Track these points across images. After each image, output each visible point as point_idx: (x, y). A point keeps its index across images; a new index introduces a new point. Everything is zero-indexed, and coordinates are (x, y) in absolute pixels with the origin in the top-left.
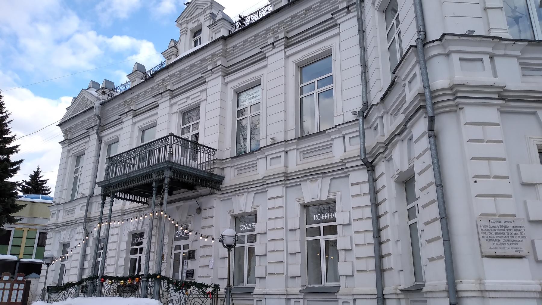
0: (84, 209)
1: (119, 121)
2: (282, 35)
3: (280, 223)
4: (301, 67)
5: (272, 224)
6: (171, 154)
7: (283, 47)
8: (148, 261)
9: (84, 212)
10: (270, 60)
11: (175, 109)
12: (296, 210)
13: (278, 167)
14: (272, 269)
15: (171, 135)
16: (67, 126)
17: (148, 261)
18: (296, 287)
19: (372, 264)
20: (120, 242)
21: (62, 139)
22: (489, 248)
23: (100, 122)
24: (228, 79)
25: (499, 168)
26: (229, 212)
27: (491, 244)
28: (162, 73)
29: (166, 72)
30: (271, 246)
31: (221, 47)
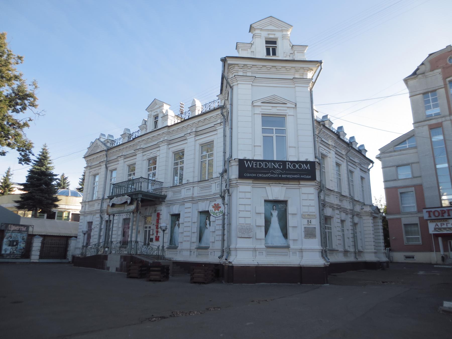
0: (100, 205)
1: (116, 160)
2: (194, 130)
3: (189, 219)
4: (202, 146)
5: (186, 220)
6: (141, 187)
7: (194, 136)
8: (132, 233)
9: (100, 206)
10: (189, 141)
11: (145, 158)
12: (196, 214)
13: (189, 194)
14: (185, 239)
15: (141, 178)
16: (89, 158)
17: (132, 233)
18: (195, 246)
19: (220, 238)
20: (119, 222)
21: (86, 165)
22: (240, 235)
23: (107, 159)
24: (170, 146)
25: (248, 208)
26: (169, 213)
27: (241, 233)
28: (138, 139)
29: (140, 138)
30: (186, 229)
31: (166, 130)
